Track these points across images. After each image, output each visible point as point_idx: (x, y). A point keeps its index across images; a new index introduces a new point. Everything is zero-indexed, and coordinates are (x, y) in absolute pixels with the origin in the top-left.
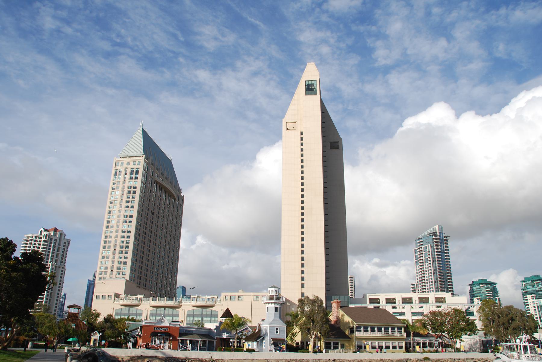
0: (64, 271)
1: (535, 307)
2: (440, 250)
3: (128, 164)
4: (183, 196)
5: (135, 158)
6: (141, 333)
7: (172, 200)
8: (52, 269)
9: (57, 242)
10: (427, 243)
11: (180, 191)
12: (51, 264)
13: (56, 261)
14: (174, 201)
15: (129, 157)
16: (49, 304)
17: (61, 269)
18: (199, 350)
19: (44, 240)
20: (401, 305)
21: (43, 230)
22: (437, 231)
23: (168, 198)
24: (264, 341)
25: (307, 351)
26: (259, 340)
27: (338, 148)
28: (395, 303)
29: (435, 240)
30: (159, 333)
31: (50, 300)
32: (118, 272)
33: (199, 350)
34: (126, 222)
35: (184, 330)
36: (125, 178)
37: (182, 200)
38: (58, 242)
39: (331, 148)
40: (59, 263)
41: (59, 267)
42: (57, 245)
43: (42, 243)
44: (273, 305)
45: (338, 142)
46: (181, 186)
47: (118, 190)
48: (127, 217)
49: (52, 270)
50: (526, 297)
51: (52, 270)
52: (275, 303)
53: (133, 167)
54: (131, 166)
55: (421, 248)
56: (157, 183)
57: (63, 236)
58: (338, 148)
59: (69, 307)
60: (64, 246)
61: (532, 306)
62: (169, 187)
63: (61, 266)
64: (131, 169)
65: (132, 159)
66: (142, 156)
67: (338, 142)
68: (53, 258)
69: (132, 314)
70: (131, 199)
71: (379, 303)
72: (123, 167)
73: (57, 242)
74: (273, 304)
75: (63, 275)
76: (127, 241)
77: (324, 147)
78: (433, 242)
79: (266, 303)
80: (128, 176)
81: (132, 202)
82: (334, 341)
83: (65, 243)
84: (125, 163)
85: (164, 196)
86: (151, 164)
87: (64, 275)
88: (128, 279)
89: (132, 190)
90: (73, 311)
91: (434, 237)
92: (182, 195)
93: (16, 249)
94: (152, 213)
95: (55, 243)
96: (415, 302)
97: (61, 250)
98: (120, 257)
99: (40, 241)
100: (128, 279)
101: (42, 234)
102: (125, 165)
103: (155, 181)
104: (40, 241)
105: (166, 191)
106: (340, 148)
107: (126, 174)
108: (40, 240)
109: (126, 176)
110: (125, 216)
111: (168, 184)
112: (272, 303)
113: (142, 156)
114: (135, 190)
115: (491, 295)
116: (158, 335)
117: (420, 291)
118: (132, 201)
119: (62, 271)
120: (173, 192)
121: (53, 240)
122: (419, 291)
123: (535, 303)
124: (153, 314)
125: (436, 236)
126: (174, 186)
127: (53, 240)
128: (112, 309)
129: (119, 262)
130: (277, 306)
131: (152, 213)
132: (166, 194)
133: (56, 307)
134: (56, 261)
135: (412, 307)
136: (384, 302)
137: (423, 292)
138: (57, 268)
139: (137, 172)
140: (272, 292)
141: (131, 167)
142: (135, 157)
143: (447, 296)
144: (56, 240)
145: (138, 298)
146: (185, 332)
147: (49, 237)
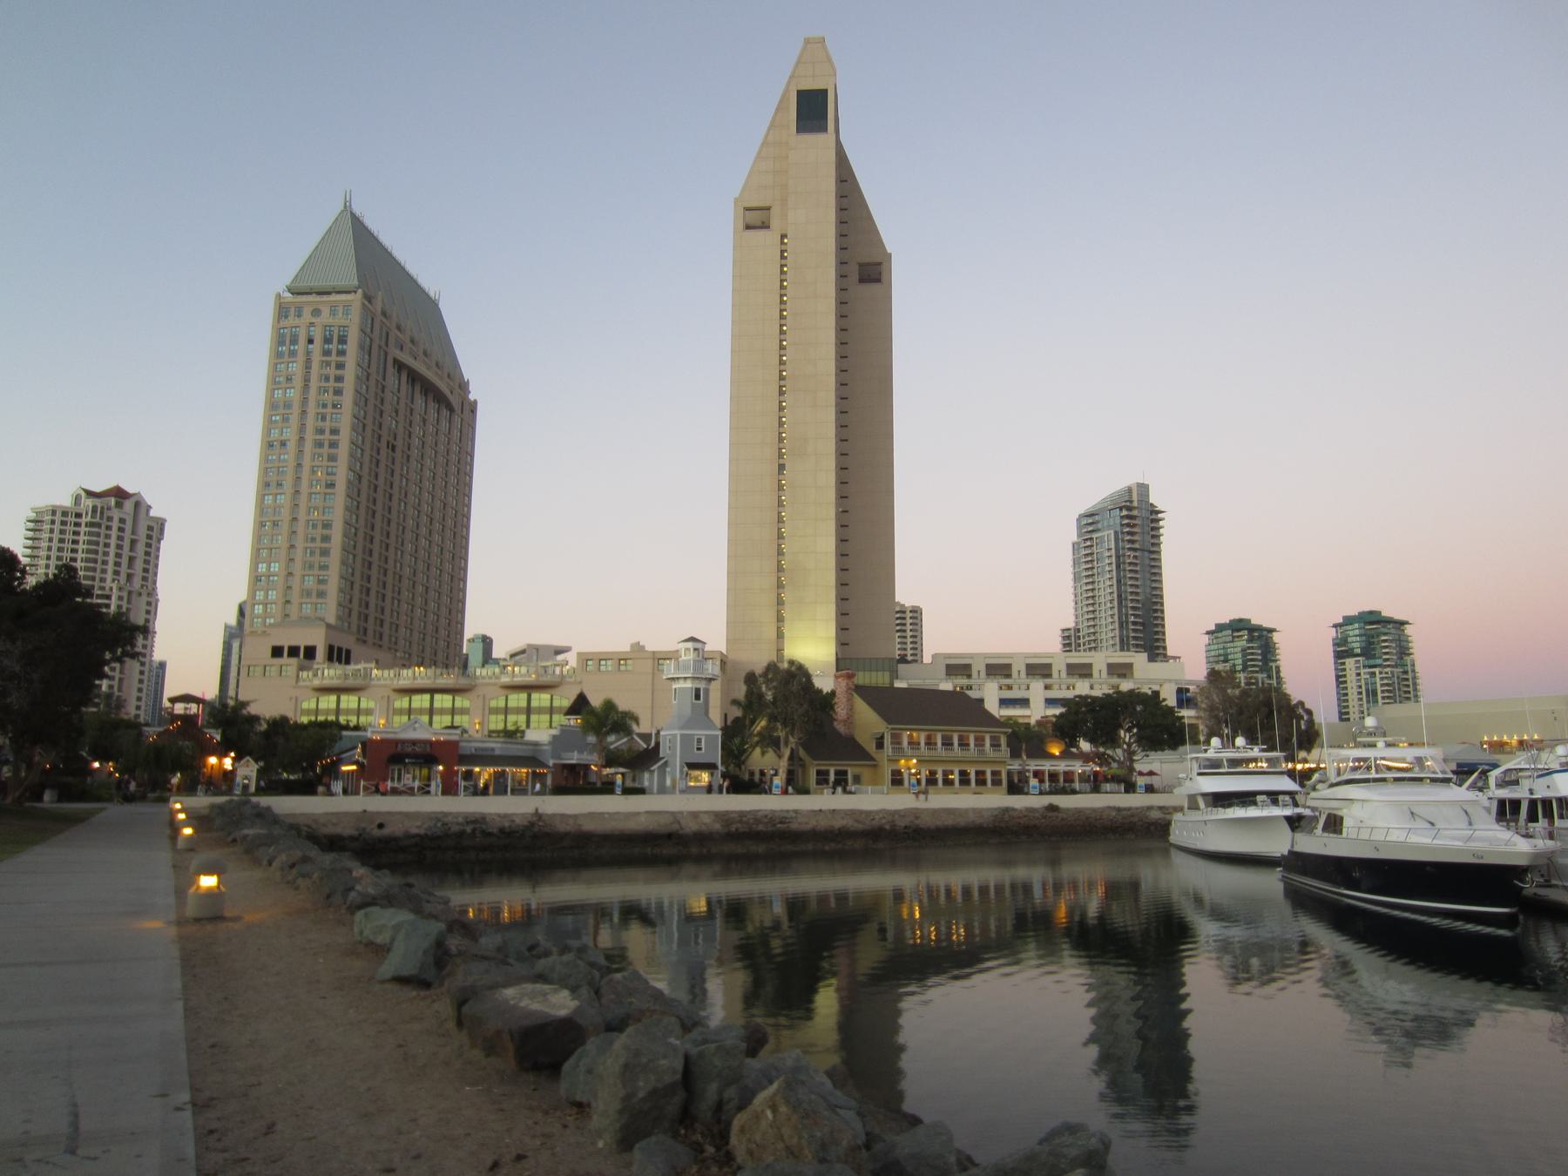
0: (153, 604)
1: (1360, 687)
2: (1137, 546)
3: (316, 312)
4: (475, 402)
5: (334, 297)
6: (364, 756)
7: (445, 412)
8: (120, 598)
9: (128, 527)
10: (1109, 527)
11: (464, 387)
12: (114, 586)
13: (130, 577)
14: (450, 415)
15: (319, 293)
16: (120, 690)
17: (144, 599)
18: (509, 793)
19: (89, 519)
20: (1023, 681)
21: (83, 494)
22: (1135, 498)
23: (432, 405)
24: (668, 769)
25: (768, 791)
26: (655, 767)
27: (878, 280)
28: (1009, 676)
29: (1126, 521)
30: (408, 756)
31: (121, 680)
32: (311, 522)
33: (509, 793)
34: (311, 567)
35: (471, 747)
36: (308, 353)
37: (472, 411)
38: (131, 527)
39: (862, 281)
40: (137, 582)
41: (140, 594)
42: (128, 535)
43: (83, 529)
44: (689, 684)
45: (879, 264)
46: (467, 374)
47: (294, 359)
48: (325, 406)
49: (120, 603)
50: (1344, 664)
51: (120, 603)
52: (693, 678)
53: (330, 321)
54: (325, 317)
55: (1091, 539)
56: (400, 366)
57: (143, 511)
58: (878, 280)
59: (173, 700)
60: (149, 537)
61: (1354, 684)
62: (430, 375)
63: (144, 591)
64: (326, 326)
65: (325, 298)
66: (355, 292)
67: (879, 264)
68: (119, 569)
69: (348, 712)
70: (329, 410)
71: (969, 676)
72: (302, 321)
73: (128, 527)
74: (689, 681)
75: (152, 614)
76: (330, 470)
77: (841, 277)
78: (1122, 525)
79: (673, 679)
80: (316, 348)
81: (324, 512)
82: (819, 768)
83: (150, 528)
84: (307, 312)
85: (419, 401)
86: (380, 312)
87: (156, 614)
88: (332, 620)
89: (319, 532)
90: (179, 708)
91: (1125, 513)
92: (472, 397)
93: (1184, 978)
94: (390, 447)
95: (121, 530)
96: (1098, 674)
97: (141, 548)
98: (321, 402)
99: (77, 524)
100: (332, 620)
101: (82, 505)
102: (307, 317)
103: (396, 361)
104: (77, 524)
105: (429, 390)
106: (884, 278)
107: (311, 341)
108: (78, 520)
109: (310, 346)
110: (305, 563)
111: (429, 368)
112: (685, 678)
113: (355, 292)
114: (341, 359)
115: (1260, 657)
116: (407, 761)
117: (1082, 648)
118: (332, 414)
119: (149, 604)
120: (447, 392)
121: (116, 520)
122: (1080, 646)
123: (1363, 676)
124: (401, 715)
125: (1129, 509)
126: (449, 376)
127: (116, 520)
128: (294, 700)
129: (308, 551)
130: (698, 686)
131: (390, 447)
132: (426, 395)
133: (139, 699)
134: (130, 577)
135: (1047, 687)
136: (983, 674)
137: (1090, 649)
138: (134, 596)
139: (343, 340)
140: (687, 652)
141: (325, 321)
142: (334, 294)
143: (1139, 660)
144: (122, 521)
145: (360, 670)
146: (473, 751)
147: (102, 513)
